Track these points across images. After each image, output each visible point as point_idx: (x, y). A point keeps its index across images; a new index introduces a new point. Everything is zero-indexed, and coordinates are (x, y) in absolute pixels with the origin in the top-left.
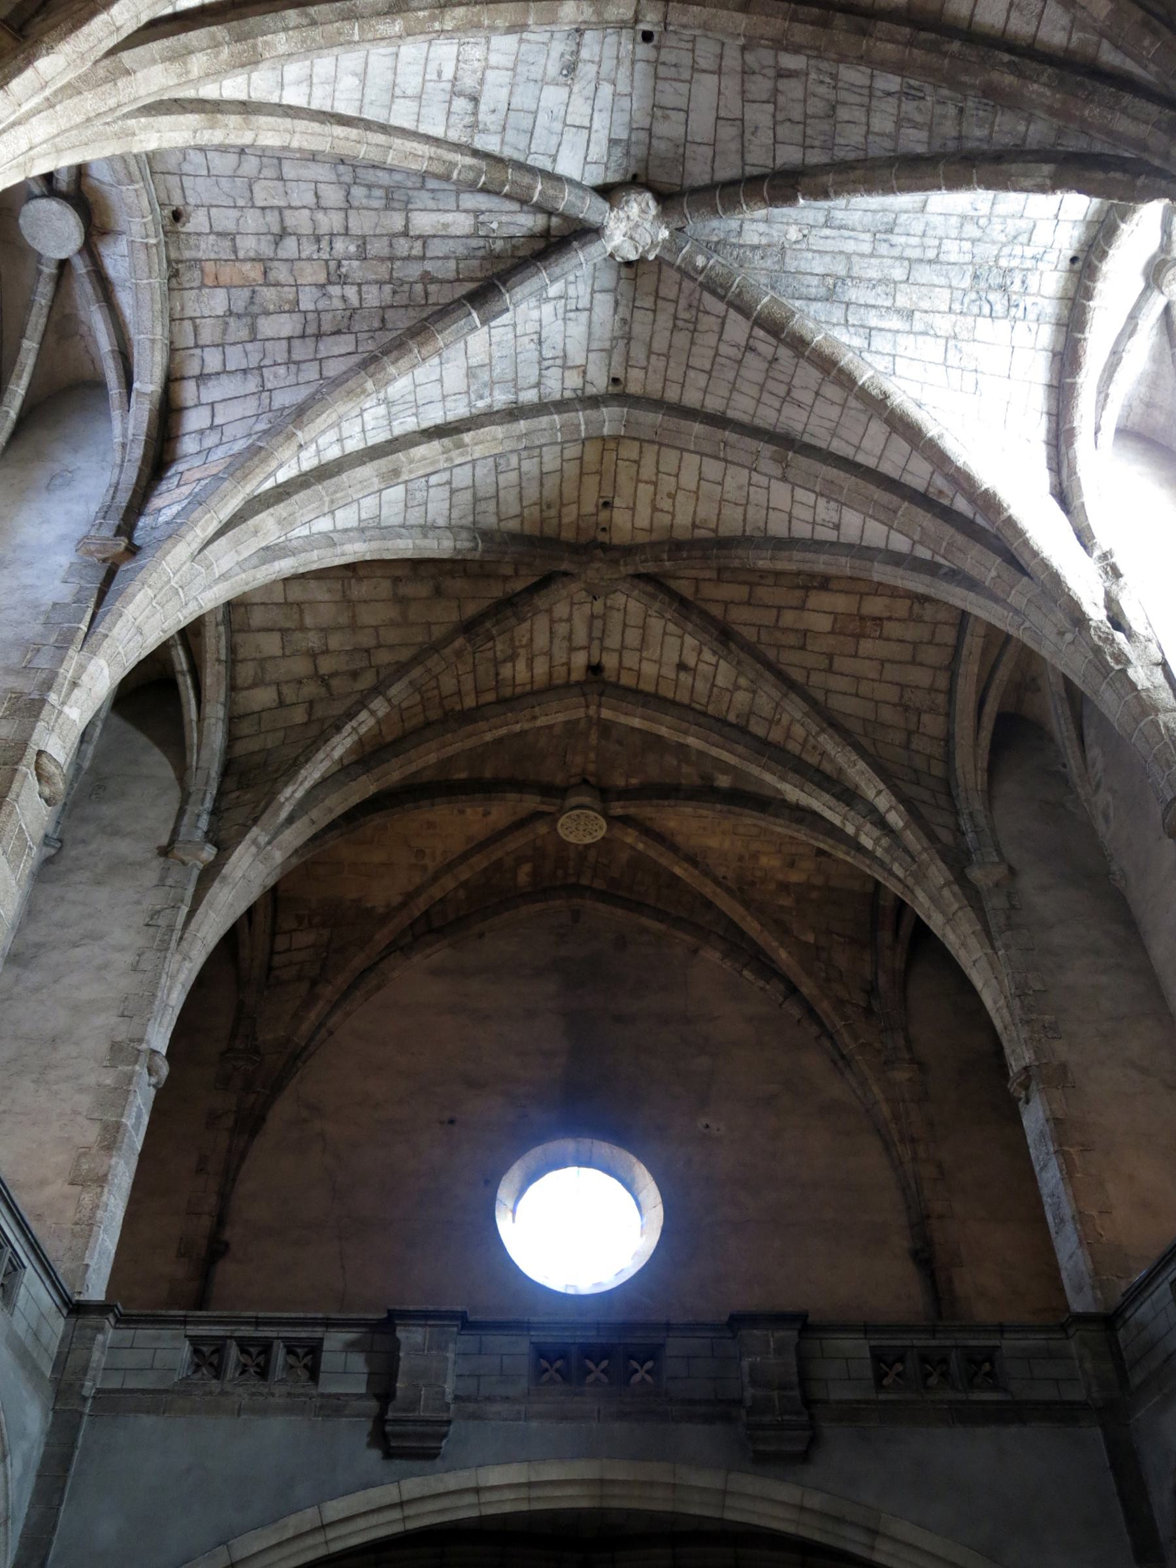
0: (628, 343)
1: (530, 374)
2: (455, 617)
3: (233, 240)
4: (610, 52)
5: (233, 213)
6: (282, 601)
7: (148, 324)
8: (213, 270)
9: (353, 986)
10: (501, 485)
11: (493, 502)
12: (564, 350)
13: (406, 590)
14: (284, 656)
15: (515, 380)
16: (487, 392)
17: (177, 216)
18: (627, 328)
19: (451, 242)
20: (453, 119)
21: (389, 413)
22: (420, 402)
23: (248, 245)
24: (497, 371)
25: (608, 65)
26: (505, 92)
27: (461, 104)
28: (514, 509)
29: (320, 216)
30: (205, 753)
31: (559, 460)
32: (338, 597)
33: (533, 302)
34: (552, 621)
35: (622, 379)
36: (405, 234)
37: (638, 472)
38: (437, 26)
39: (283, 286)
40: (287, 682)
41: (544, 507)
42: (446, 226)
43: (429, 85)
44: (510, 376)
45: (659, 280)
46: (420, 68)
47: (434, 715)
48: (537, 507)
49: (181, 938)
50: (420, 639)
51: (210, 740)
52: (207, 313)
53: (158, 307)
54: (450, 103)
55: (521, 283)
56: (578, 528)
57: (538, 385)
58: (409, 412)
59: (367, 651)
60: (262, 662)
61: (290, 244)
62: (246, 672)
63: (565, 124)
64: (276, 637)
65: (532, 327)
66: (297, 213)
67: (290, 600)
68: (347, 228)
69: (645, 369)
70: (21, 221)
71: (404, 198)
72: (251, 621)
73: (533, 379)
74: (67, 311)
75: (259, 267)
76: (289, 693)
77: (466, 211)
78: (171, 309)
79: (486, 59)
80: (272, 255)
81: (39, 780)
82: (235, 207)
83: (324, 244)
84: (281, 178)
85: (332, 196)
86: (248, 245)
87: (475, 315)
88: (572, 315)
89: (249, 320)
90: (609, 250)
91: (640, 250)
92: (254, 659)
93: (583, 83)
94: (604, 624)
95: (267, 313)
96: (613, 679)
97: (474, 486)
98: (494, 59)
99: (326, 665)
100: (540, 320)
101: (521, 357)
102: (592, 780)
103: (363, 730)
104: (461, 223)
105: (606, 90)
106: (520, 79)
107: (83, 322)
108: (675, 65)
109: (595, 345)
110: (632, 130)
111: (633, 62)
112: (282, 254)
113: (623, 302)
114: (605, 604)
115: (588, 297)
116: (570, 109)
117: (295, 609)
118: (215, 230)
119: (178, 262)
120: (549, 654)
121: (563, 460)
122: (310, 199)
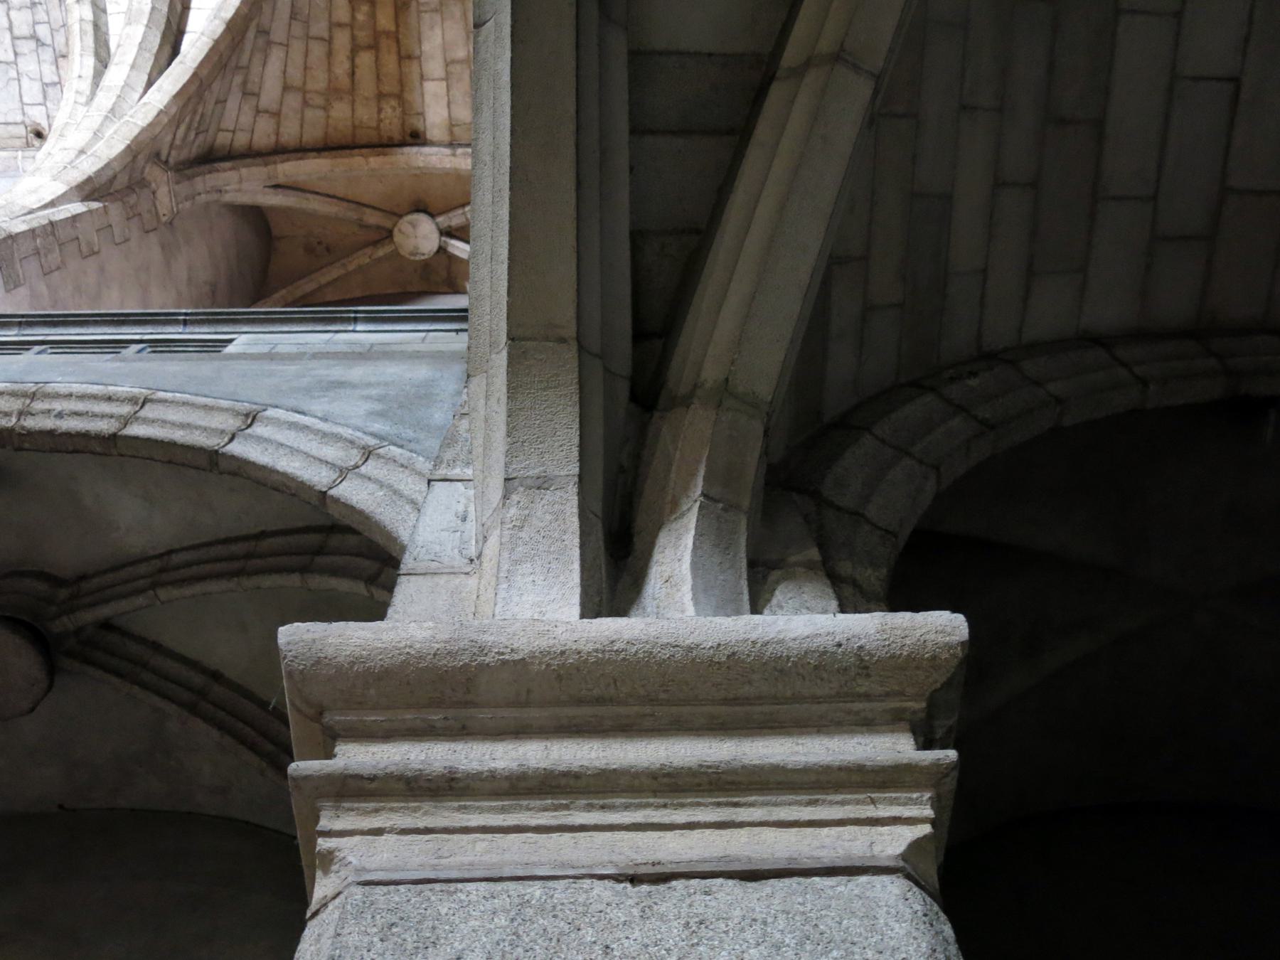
5: (25, 82)
6: (444, 84)
9: (123, 566)
32: (437, 18)
61: (43, 31)
66: (15, 23)
67: (443, 75)
117: (451, 68)
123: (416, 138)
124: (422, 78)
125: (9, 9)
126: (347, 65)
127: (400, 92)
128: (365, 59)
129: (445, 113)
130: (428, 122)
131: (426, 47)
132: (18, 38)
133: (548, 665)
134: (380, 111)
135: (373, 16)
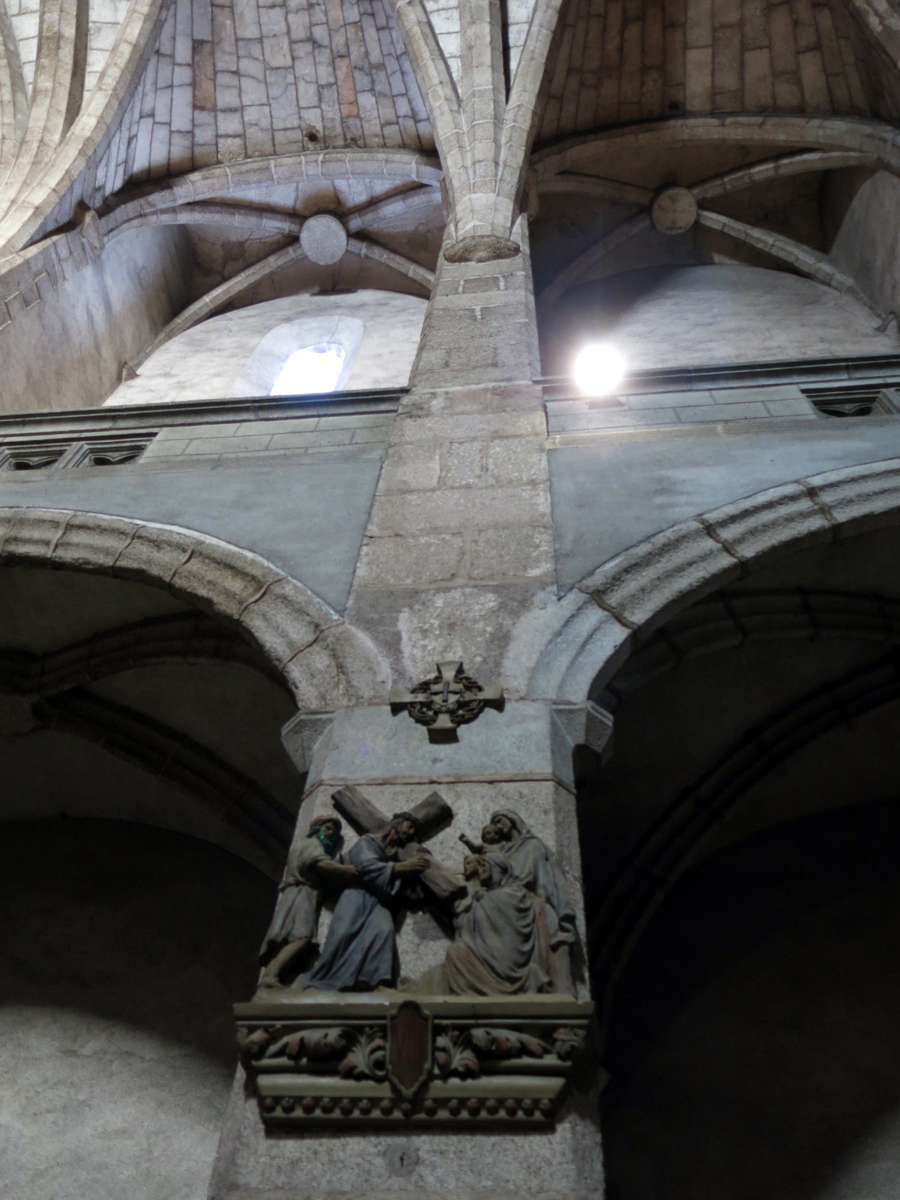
3: (323, 87)
5: (302, 85)
6: (710, 50)
8: (346, 106)
23: (325, 74)
30: (851, 141)
39: (347, 39)
40: (796, 42)
52: (375, 113)
53: (365, 155)
60: (776, 73)
61: (320, 33)
62: (786, 94)
64: (749, 57)
66: (293, 27)
67: (709, 41)
70: (322, 263)
72: (733, 88)
76: (807, 37)
78: (378, 146)
80: (328, 51)
81: (467, 260)
82: (296, 84)
84: (260, 40)
86: (325, 74)
92: (773, 85)
95: (367, 54)
107: (416, 229)
119: (345, 139)
123: (676, 110)
124: (686, 47)
125: (287, 13)
127: (663, 65)
128: (634, 31)
129: (708, 80)
130: (688, 93)
131: (692, 13)
134: (642, 84)
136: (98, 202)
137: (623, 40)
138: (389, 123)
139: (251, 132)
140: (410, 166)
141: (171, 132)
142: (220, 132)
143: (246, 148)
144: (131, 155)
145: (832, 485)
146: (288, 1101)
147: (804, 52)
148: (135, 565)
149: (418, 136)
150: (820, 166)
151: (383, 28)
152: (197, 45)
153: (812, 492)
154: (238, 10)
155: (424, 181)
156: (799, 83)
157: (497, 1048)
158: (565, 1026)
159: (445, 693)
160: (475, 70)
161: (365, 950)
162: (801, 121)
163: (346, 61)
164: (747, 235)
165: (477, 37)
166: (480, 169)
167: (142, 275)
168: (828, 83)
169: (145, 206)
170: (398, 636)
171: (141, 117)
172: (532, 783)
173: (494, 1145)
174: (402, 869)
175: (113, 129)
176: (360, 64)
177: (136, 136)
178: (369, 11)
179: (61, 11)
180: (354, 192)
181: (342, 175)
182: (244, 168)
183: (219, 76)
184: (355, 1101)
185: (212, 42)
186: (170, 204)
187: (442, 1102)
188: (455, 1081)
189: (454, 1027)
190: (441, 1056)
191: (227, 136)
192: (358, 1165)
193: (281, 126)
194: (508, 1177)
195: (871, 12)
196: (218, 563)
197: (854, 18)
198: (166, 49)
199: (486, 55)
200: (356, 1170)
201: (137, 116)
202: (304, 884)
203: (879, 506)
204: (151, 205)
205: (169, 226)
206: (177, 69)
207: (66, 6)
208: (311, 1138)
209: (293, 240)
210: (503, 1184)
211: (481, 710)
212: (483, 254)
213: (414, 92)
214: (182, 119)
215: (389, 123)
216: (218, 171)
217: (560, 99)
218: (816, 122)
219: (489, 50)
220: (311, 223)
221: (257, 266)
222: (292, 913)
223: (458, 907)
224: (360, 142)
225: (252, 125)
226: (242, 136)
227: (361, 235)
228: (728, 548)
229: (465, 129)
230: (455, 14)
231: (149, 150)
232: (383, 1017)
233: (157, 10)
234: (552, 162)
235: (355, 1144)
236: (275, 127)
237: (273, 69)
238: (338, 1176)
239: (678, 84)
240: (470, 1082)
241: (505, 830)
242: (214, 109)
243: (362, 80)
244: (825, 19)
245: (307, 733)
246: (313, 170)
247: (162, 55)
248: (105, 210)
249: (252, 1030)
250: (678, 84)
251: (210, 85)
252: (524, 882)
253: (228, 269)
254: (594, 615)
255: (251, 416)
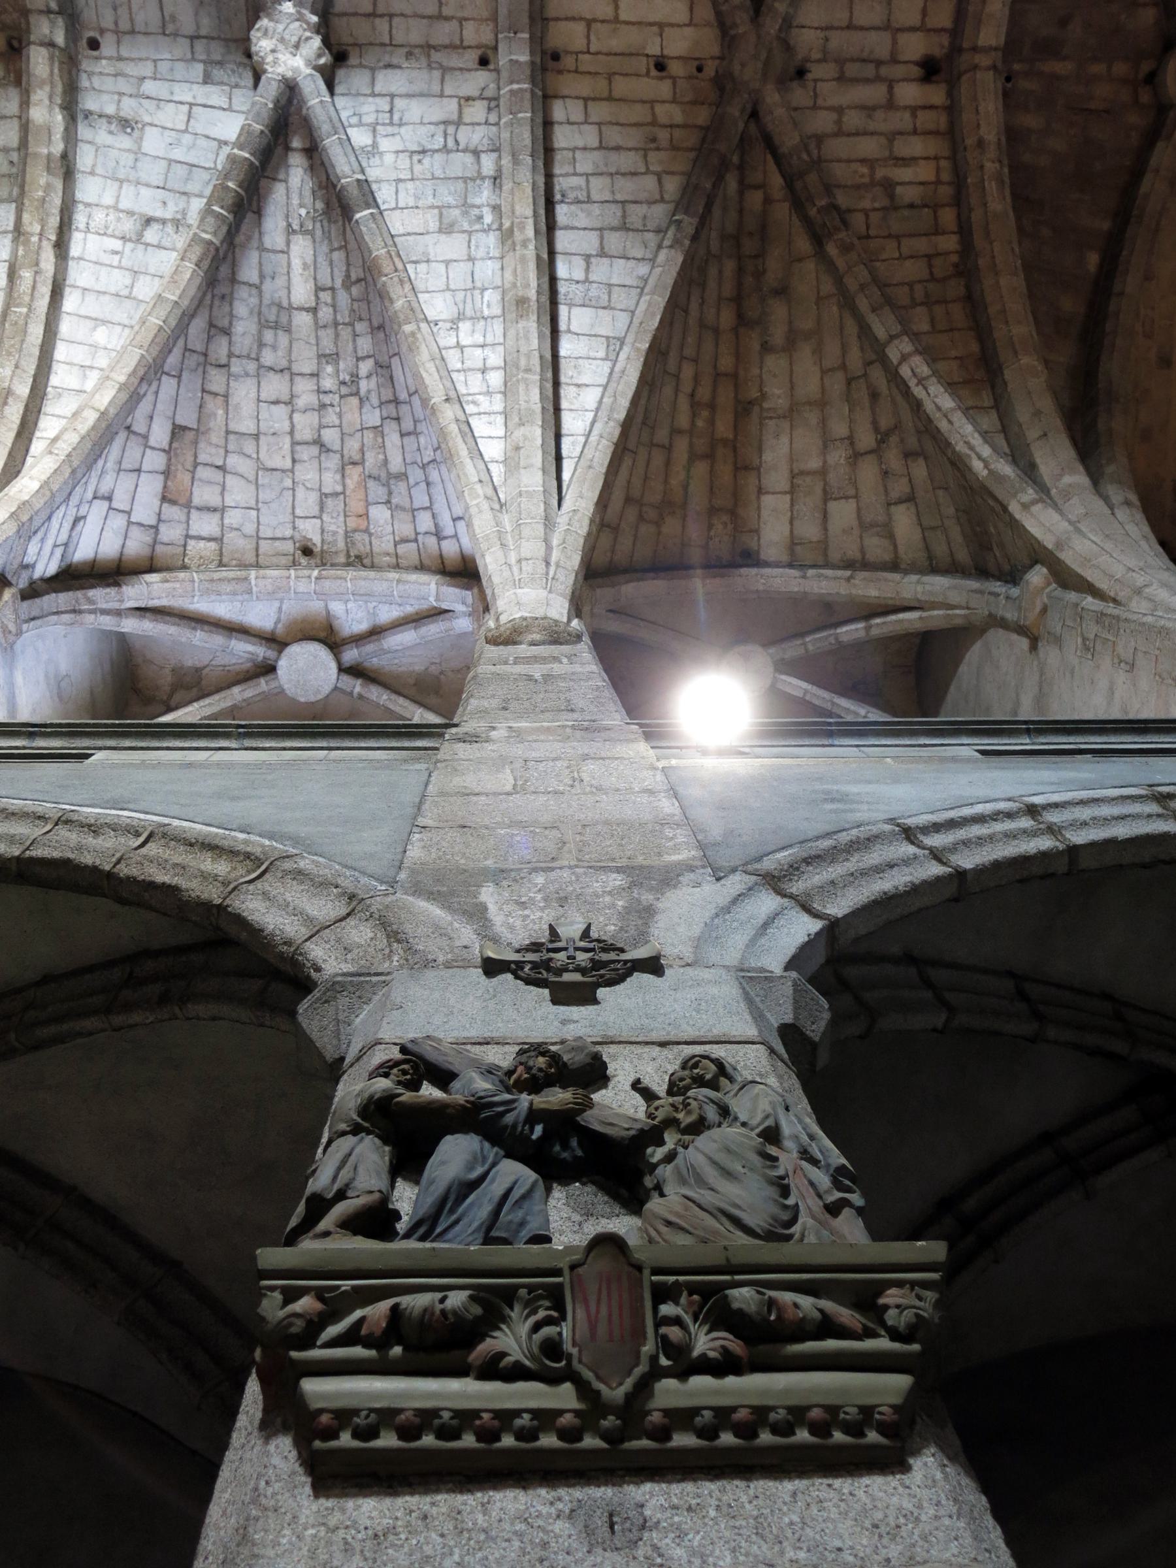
0: (434, 47)
1: (461, 163)
2: (810, 266)
3: (326, 495)
4: (109, 84)
5: (301, 493)
6: (788, 497)
7: (385, 585)
10: (608, 197)
11: (631, 208)
12: (437, 124)
13: (778, 334)
14: (856, 497)
15: (465, 180)
16: (476, 212)
17: (307, 551)
18: (416, 51)
19: (320, 259)
20: (164, 243)
21: (472, 318)
22: (470, 285)
23: (331, 482)
24: (450, 200)
25: (122, 85)
26: (144, 191)
27: (151, 235)
28: (650, 182)
29: (301, 403)
30: (955, 598)
31: (586, 127)
32: (786, 425)
33: (375, 161)
34: (839, 133)
35: (479, 52)
36: (314, 311)
37: (603, 21)
38: (35, 239)
41: (652, 146)
42: (305, 266)
43: (124, 263)
44: (460, 185)
45: (355, 14)
46: (104, 270)
47: (956, 288)
48: (651, 154)
49: (1115, 601)
50: (835, 309)
51: (944, 596)
52: (389, 529)
54: (147, 245)
55: (333, 166)
56: (694, 103)
57: (476, 153)
58: (478, 296)
59: (849, 382)
61: (330, 436)
62: (877, 548)
63: (186, 131)
64: (833, 506)
65: (404, 162)
66: (298, 427)
67: (787, 488)
68: (312, 375)
69: (461, 20)
70: (302, 700)
71: (274, 310)
73: (469, 159)
74: (412, 681)
75: (349, 469)
76: (899, 488)
77: (288, 243)
79: (108, 207)
81: (515, 643)
83: (327, 399)
84: (256, 436)
85: (275, 386)
86: (331, 482)
87: (358, 216)
88: (396, 117)
89: (392, 482)
90: (309, 71)
91: (308, 34)
93: (142, 111)
94: (853, 60)
95: (386, 462)
96: (945, 40)
97: (601, 229)
98: (108, 200)
99: (866, 439)
100: (397, 152)
101: (439, 173)
102: (1146, 67)
103: (925, 370)
104: (301, 249)
105: (149, 87)
106: (133, 176)
108: (115, 9)
109: (436, 88)
110: (193, 59)
111: (120, 59)
112: (337, 447)
113: (386, 59)
114: (819, 61)
115: (378, 100)
116: (169, 125)
118: (317, 513)
119: (348, 556)
120: (891, 137)
121: (586, 122)
122: (281, 411)
124: (760, 491)
126: (682, 476)
131: (768, 456)
132: (299, 444)
133: (838, 1176)
135: (712, 422)
136: (23, 583)
137: (688, 477)
138: (405, 541)
139: (229, 537)
140: (430, 589)
141: (130, 523)
142: (191, 533)
143: (221, 555)
144: (75, 540)
145: (1056, 805)
146: (367, 1416)
147: (895, 504)
148: (56, 854)
149: (441, 556)
150: (919, 626)
151: (409, 434)
152: (178, 431)
153: (1032, 811)
154: (233, 401)
155: (444, 606)
156: (891, 537)
157: (779, 1318)
158: (900, 1284)
159: (571, 950)
160: (522, 471)
161: (496, 1200)
162: (897, 576)
163: (359, 469)
164: (833, 703)
165: (525, 438)
166: (527, 567)
167: (63, 684)
168: (924, 538)
169: (82, 601)
170: (483, 908)
171: (95, 498)
172: (729, 1046)
173: (794, 1494)
174: (543, 1106)
175: (58, 500)
176: (375, 472)
177: (84, 517)
178: (394, 415)
179: (17, 367)
180: (352, 617)
181: (340, 596)
182: (216, 576)
183: (199, 468)
184: (505, 1417)
185: (197, 430)
186: (115, 605)
187: (683, 1418)
188: (701, 1381)
189: (692, 1289)
190: (674, 1333)
191: (200, 538)
192: (520, 1535)
193: (269, 534)
194: (838, 1543)
195: (973, 455)
196: (191, 845)
197: (953, 464)
198: (140, 427)
199: (535, 456)
200: (516, 1544)
201: (89, 495)
202: (369, 1133)
203: (1122, 831)
204: (90, 601)
205: (104, 632)
206: (148, 451)
207: (23, 363)
208: (412, 1494)
209: (269, 669)
210: (830, 1556)
211: (629, 973)
212: (537, 637)
213: (440, 505)
214: (146, 508)
215: (405, 541)
216: (182, 575)
217: (615, 530)
218: (914, 578)
219: (539, 453)
220: (295, 649)
221: (216, 697)
222: (352, 1159)
223: (652, 1155)
224: (367, 561)
225: (232, 529)
226: (219, 540)
227: (355, 671)
228: (936, 855)
229: (509, 529)
230: (500, 419)
231: (97, 541)
232: (557, 1272)
233: (136, 381)
234: (605, 594)
235: (508, 1502)
236: (261, 535)
237: (267, 470)
238: (479, 1555)
239: (751, 531)
240: (731, 1381)
241: (708, 1077)
242: (188, 506)
243: (377, 491)
244: (920, 470)
245: (343, 1001)
246: (303, 586)
247: (134, 433)
248: (31, 592)
249: (291, 1295)
250: (751, 531)
251: (187, 477)
252: (758, 1131)
253: (177, 697)
254: (767, 902)
255: (234, 744)
